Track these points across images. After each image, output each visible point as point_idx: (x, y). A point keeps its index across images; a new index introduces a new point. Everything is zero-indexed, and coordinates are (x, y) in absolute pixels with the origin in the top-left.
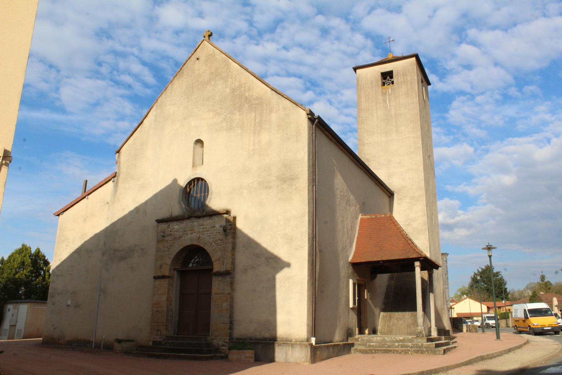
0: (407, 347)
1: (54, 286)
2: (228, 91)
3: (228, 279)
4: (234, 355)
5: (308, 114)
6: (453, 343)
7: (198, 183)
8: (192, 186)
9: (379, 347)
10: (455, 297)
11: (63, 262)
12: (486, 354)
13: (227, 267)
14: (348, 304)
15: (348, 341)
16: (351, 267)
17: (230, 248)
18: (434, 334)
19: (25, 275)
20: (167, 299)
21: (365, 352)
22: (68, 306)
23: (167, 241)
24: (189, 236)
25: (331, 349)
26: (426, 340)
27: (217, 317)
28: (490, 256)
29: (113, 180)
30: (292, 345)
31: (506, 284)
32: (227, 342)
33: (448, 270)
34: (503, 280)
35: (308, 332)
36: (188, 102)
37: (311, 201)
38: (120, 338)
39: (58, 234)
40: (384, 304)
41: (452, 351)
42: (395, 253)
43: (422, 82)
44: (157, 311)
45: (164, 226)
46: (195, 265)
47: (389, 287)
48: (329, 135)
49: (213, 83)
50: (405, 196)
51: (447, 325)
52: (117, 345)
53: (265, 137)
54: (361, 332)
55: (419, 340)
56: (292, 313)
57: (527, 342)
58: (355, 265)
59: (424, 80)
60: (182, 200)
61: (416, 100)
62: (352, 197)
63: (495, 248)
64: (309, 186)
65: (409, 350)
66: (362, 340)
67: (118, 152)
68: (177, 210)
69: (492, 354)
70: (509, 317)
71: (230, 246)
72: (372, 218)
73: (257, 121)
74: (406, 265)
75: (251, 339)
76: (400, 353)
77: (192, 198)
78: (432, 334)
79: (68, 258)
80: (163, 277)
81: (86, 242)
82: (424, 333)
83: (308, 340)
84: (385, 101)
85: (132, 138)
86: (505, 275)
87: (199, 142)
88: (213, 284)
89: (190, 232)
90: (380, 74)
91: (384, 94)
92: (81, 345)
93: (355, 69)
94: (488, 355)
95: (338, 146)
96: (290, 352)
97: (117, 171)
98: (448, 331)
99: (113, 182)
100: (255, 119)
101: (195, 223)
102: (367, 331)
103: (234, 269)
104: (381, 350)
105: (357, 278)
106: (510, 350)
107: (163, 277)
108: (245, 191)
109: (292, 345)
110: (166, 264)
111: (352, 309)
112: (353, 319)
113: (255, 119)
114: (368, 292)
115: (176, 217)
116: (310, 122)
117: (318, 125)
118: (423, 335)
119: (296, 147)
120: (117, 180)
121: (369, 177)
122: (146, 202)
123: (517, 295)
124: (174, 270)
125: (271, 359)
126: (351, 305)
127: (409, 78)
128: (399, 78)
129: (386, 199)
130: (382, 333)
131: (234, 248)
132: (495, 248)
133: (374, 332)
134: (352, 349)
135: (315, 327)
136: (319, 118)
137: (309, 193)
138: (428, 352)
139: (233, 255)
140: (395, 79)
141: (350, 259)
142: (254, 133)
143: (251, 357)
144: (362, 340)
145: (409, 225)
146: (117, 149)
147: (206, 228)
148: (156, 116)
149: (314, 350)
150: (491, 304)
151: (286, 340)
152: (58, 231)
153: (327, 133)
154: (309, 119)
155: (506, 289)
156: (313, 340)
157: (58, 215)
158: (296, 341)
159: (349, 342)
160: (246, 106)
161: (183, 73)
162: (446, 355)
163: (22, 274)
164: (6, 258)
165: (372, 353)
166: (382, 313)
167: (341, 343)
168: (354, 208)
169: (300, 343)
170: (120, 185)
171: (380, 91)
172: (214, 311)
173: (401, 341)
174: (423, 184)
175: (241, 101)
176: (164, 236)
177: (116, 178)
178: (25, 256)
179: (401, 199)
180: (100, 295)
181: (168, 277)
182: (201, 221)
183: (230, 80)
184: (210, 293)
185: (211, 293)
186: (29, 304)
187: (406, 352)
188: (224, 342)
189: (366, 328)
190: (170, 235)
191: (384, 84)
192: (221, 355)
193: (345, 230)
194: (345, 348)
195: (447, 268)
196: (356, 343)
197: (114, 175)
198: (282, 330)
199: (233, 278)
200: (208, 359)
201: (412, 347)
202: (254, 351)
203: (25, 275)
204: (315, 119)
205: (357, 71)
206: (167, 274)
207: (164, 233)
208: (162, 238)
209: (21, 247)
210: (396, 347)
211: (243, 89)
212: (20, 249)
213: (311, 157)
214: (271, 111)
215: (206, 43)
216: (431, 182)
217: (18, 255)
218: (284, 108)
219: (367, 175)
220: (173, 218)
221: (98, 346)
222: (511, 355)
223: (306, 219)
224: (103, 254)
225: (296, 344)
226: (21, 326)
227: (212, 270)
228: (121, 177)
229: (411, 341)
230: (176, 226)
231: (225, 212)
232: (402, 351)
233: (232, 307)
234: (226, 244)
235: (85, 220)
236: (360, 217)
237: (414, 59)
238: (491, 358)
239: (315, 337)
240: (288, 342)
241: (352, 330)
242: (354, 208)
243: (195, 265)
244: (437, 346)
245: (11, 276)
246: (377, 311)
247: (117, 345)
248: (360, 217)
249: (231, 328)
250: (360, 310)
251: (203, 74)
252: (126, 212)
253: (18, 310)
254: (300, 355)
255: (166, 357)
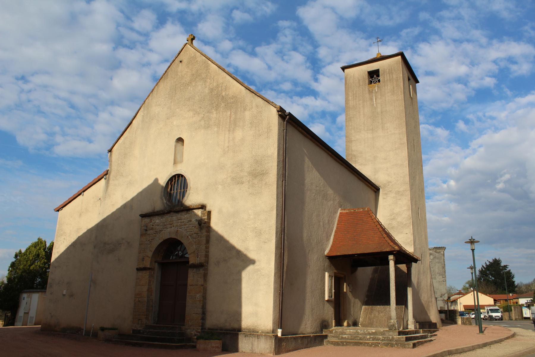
0: (378, 339)
1: (53, 275)
2: (207, 91)
3: (202, 271)
4: (201, 344)
5: (278, 111)
6: (431, 336)
7: (178, 181)
8: (173, 183)
9: (351, 339)
10: (464, 289)
11: (61, 255)
12: (455, 348)
13: (202, 259)
14: (324, 297)
15: (322, 333)
16: (328, 260)
17: (204, 241)
18: (411, 327)
19: (39, 266)
20: (148, 290)
21: (337, 344)
22: (64, 295)
23: (149, 234)
24: (169, 229)
25: (299, 341)
26: (397, 334)
27: (192, 309)
28: (473, 250)
29: (105, 177)
30: (258, 336)
31: (513, 277)
32: (199, 332)
33: (446, 263)
34: (511, 273)
35: (274, 323)
36: (171, 102)
37: (280, 196)
38: (105, 326)
39: (57, 229)
40: (367, 296)
41: (426, 344)
42: (369, 246)
43: (409, 79)
44: (139, 301)
45: (147, 220)
46: (174, 257)
47: (372, 279)
48: (303, 131)
49: (194, 84)
50: (390, 191)
51: (434, 317)
52: (101, 333)
53: (239, 134)
54: (339, 323)
55: (391, 333)
56: (257, 304)
57: (513, 335)
58: (332, 259)
59: (411, 77)
60: (164, 196)
61: (401, 97)
62: (330, 192)
63: (478, 242)
64: (278, 181)
65: (380, 343)
66: (336, 332)
67: (110, 151)
68: (159, 205)
69: (462, 348)
70: (511, 310)
71: (204, 240)
72: (351, 213)
73: (232, 119)
74: (379, 259)
75: (221, 329)
76: (371, 346)
77: (172, 193)
78: (409, 327)
79: (65, 251)
80: (145, 269)
81: (79, 237)
82: (396, 326)
83: (274, 331)
84: (371, 99)
85: (122, 138)
86: (512, 268)
87: (180, 140)
88: (189, 275)
89: (169, 226)
90: (367, 73)
91: (370, 92)
92: (73, 333)
93: (343, 69)
94: (457, 350)
95: (314, 142)
96: (256, 343)
97: (109, 169)
98: (435, 324)
99: (105, 179)
100: (230, 117)
101: (174, 218)
102: (345, 324)
103: (207, 262)
104: (352, 343)
105: (335, 271)
106: (485, 345)
107: (145, 269)
108: (220, 187)
109: (258, 337)
110: (147, 256)
111: (328, 301)
112: (329, 312)
113: (230, 117)
114: (348, 285)
115: (157, 212)
116: (280, 119)
117: (288, 120)
118: (395, 327)
119: (265, 142)
120: (109, 177)
121: (351, 172)
122: (133, 199)
123: (523, 288)
124: (155, 262)
125: (235, 349)
126: (327, 298)
127: (394, 76)
128: (385, 76)
129: (371, 194)
130: (363, 326)
131: (208, 241)
132: (478, 242)
133: (355, 324)
134: (325, 340)
135: (281, 319)
136: (290, 114)
137: (277, 188)
138: (398, 346)
139: (207, 248)
140: (381, 78)
141: (326, 253)
142: (229, 131)
143: (218, 347)
144: (336, 332)
145: (394, 219)
146: (109, 148)
147: (184, 222)
148: (143, 116)
149: (279, 341)
150: (498, 297)
151: (253, 332)
152: (57, 226)
153: (300, 129)
154: (279, 115)
155: (514, 282)
156: (279, 333)
157: (58, 211)
158: (262, 332)
159: (324, 334)
160: (223, 105)
161: (167, 75)
162: (415, 349)
163: (36, 266)
164: (23, 251)
165: (343, 345)
166: (363, 307)
167: (312, 335)
168: (332, 202)
169: (265, 334)
170: (111, 182)
171: (367, 89)
172: (189, 301)
173: (373, 334)
174: (407, 179)
175: (218, 100)
176: (146, 230)
177: (107, 176)
178: (40, 249)
179: (386, 194)
180: (91, 286)
181: (149, 269)
182: (179, 215)
183: (209, 80)
184: (186, 285)
185: (187, 285)
186: (40, 293)
187: (376, 345)
188: (197, 332)
189: (345, 320)
190: (152, 229)
191: (371, 83)
192: (192, 344)
193: (321, 224)
194: (318, 339)
195: (444, 262)
196: (329, 335)
197: (106, 173)
198: (247, 321)
199: (206, 270)
200: (177, 348)
201: (382, 340)
202: (221, 341)
203: (39, 266)
204: (287, 116)
205: (346, 70)
206: (149, 266)
207: (147, 227)
208: (145, 231)
209: (37, 241)
210: (368, 340)
211: (220, 89)
212: (36, 243)
213: (281, 152)
214: (245, 110)
215: (188, 46)
216: (417, 177)
217: (33, 248)
218: (257, 106)
219: (349, 170)
220: (154, 212)
221: (88, 333)
222: (486, 350)
223: (275, 212)
224: (95, 247)
225: (262, 335)
226: (33, 313)
227: (188, 262)
228: (112, 175)
229: (383, 334)
230: (157, 220)
231: (200, 207)
232: (372, 344)
233: (204, 298)
234: (201, 237)
235: (80, 215)
236: (339, 211)
237: (400, 57)
238: (460, 353)
239: (281, 328)
240: (253, 333)
241: (328, 322)
242: (332, 202)
243: (174, 257)
244: (408, 339)
245: (27, 267)
246: (358, 302)
247: (101, 333)
248: (339, 211)
249: (203, 318)
250: (339, 303)
251: (185, 76)
252: (114, 210)
253: (31, 299)
254: (265, 346)
255: (140, 345)
